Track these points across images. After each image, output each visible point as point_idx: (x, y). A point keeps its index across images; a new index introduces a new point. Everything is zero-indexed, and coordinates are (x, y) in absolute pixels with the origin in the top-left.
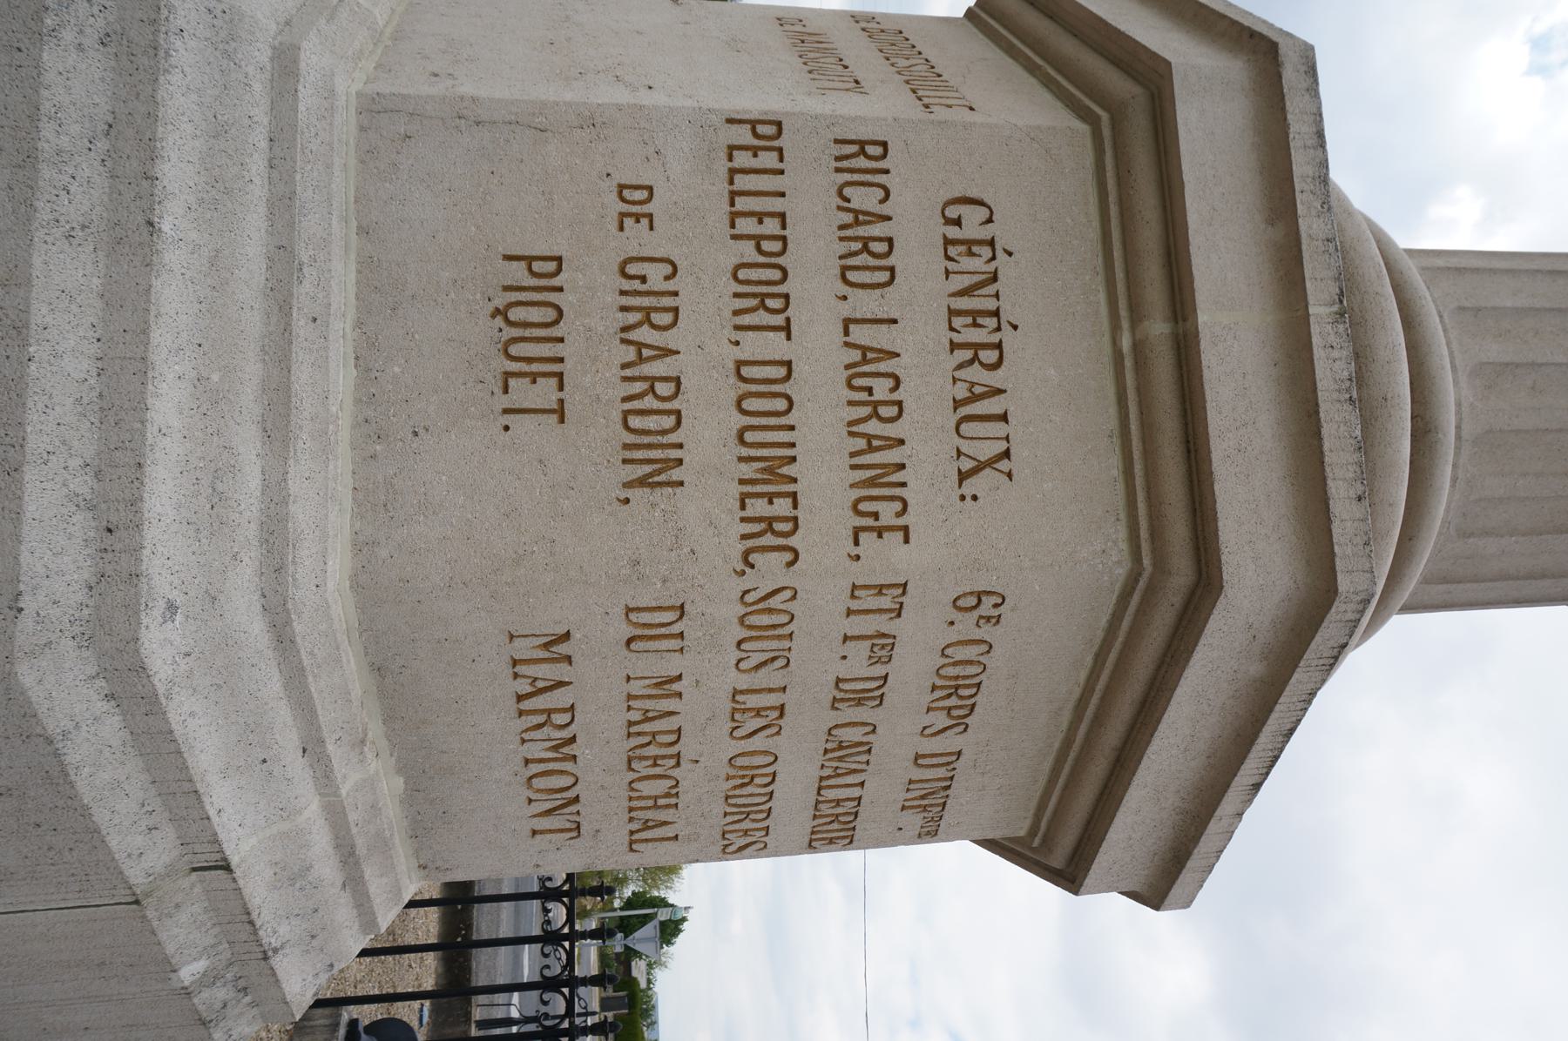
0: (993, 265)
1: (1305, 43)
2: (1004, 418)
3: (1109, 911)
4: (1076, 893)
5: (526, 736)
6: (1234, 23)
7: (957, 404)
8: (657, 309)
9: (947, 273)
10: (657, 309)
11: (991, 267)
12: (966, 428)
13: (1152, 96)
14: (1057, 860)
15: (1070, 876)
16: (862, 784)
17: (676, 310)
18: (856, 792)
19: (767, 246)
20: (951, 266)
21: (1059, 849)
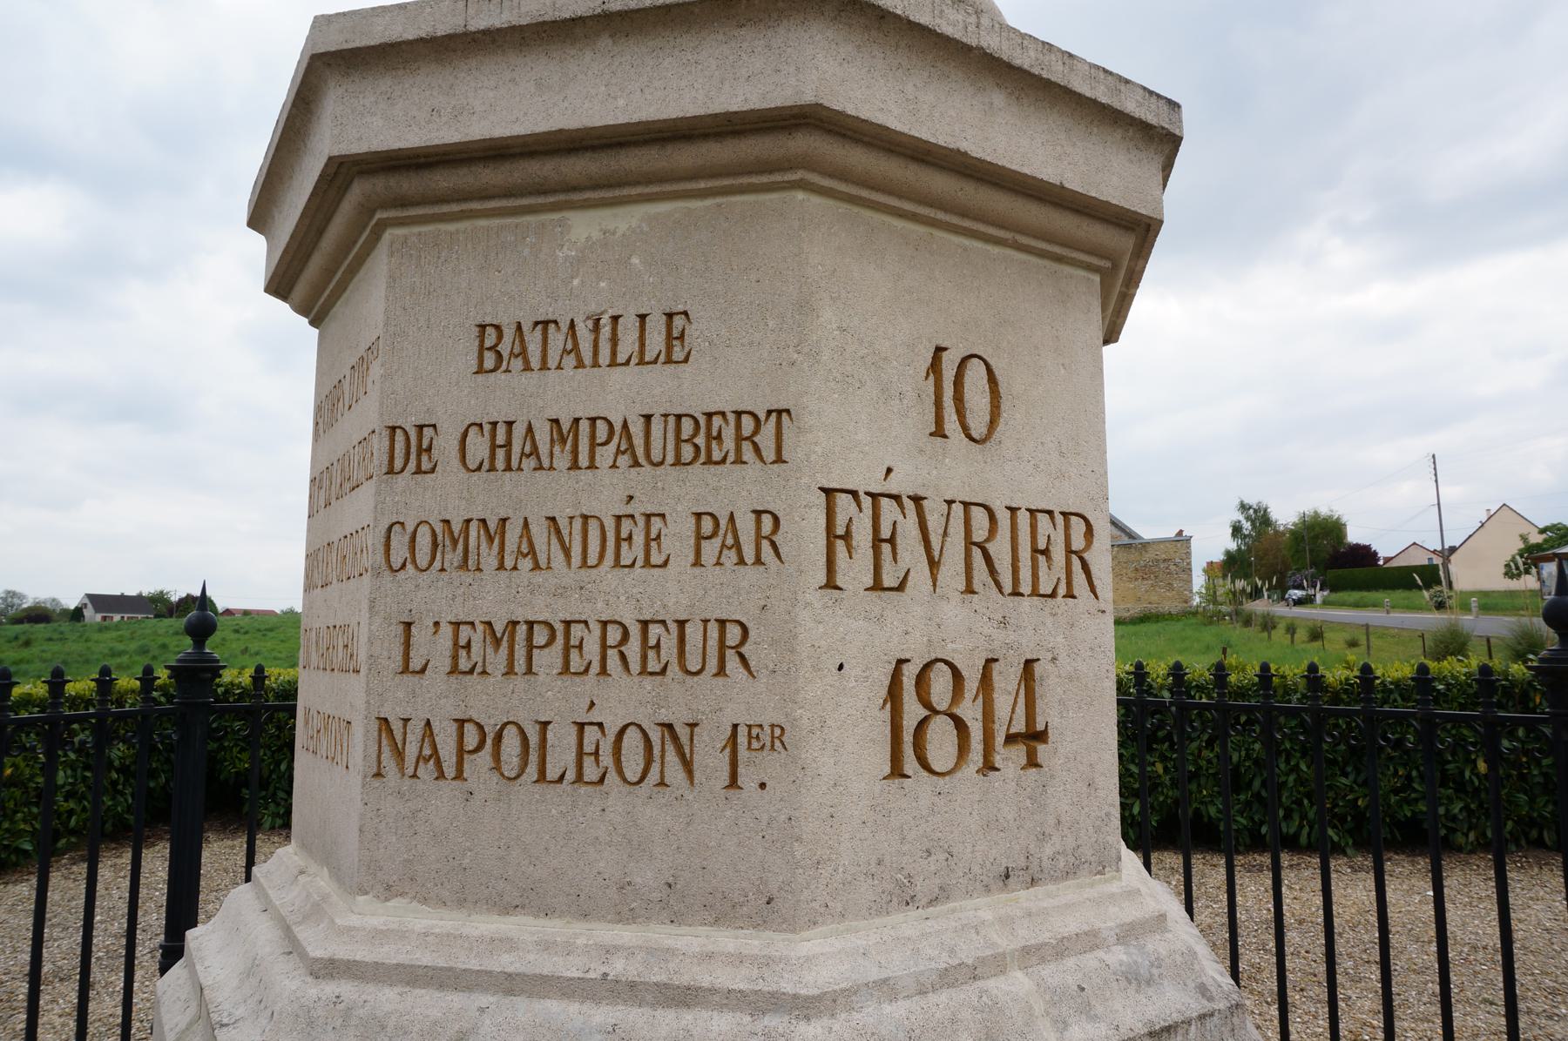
0: (477, 623)
1: (313, 27)
2: (648, 418)
3: (1183, 198)
4: (1161, 222)
5: (1008, 588)
6: (294, 105)
7: (636, 464)
8: (593, 436)
9: (484, 672)
10: (593, 436)
11: (480, 628)
12: (656, 455)
13: (361, 173)
14: (1126, 242)
15: (1143, 231)
16: (1013, 510)
17: (593, 420)
18: (1023, 519)
19: (471, 740)
20: (479, 669)
21: (1111, 250)
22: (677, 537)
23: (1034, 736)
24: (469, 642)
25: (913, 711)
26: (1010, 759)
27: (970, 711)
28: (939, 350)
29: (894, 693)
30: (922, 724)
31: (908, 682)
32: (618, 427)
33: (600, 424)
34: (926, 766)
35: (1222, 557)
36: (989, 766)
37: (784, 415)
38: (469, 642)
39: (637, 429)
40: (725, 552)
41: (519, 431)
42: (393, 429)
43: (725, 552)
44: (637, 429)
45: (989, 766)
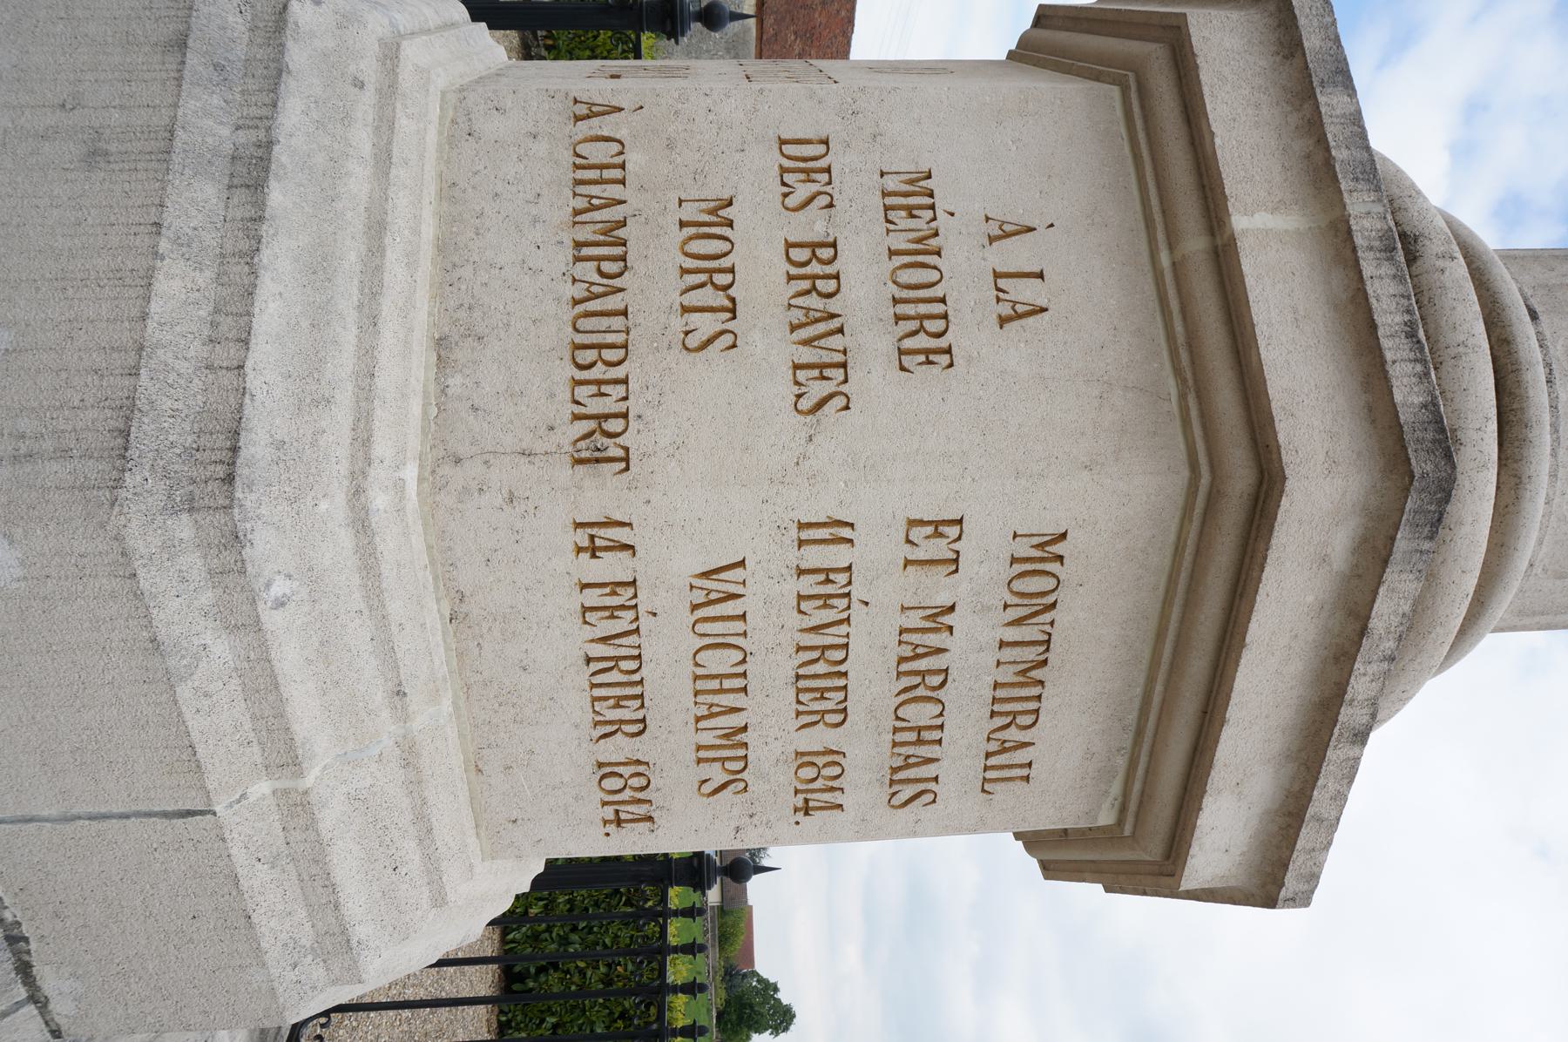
17: (945, 316)
22: (813, 225)
23: (619, 822)
24: (832, 582)
25: (820, 761)
26: (609, 812)
27: (818, 784)
28: (852, 525)
29: (638, 762)
30: (814, 764)
31: (641, 769)
32: (617, 282)
33: (729, 277)
34: (800, 767)
35: (785, 1002)
36: (604, 804)
37: (623, 465)
38: (832, 582)
39: (613, 303)
40: (910, 648)
41: (614, 191)
42: (826, 142)
43: (910, 648)
44: (613, 303)
45: (604, 804)
